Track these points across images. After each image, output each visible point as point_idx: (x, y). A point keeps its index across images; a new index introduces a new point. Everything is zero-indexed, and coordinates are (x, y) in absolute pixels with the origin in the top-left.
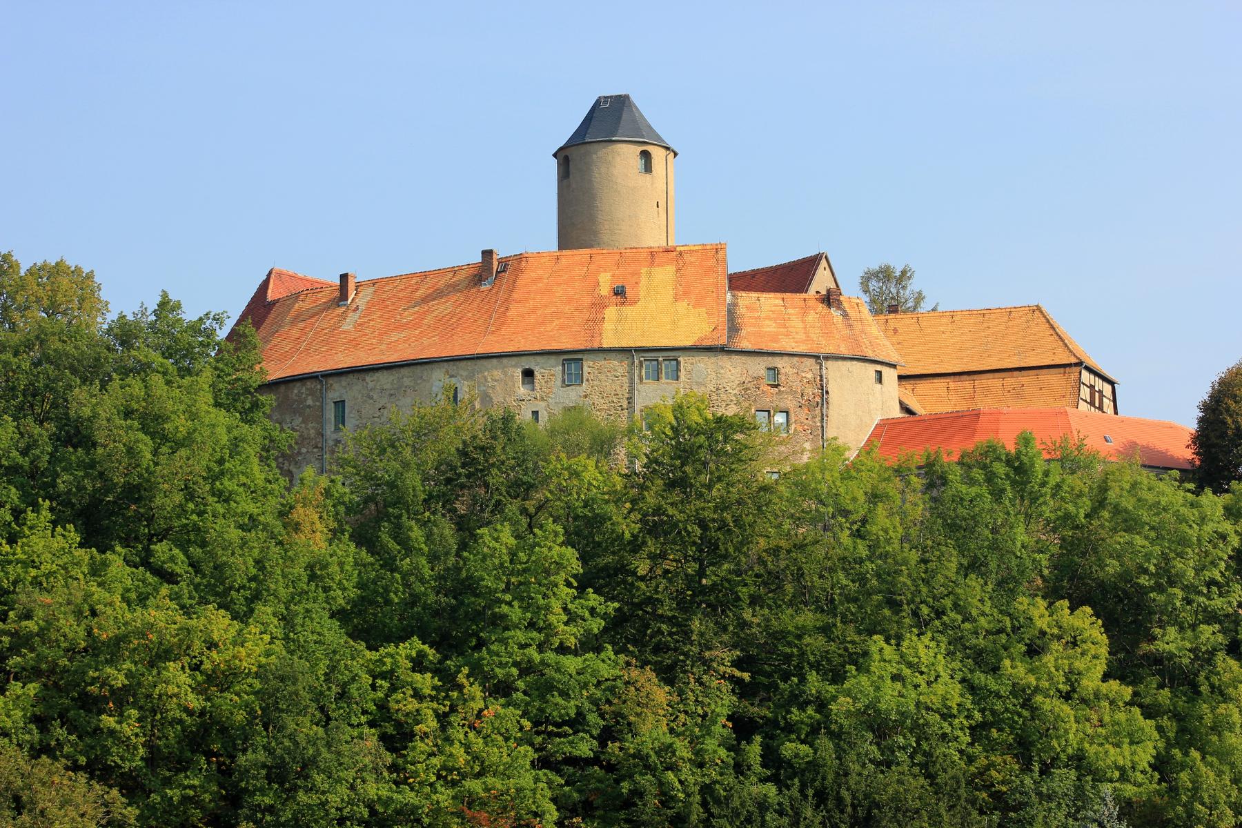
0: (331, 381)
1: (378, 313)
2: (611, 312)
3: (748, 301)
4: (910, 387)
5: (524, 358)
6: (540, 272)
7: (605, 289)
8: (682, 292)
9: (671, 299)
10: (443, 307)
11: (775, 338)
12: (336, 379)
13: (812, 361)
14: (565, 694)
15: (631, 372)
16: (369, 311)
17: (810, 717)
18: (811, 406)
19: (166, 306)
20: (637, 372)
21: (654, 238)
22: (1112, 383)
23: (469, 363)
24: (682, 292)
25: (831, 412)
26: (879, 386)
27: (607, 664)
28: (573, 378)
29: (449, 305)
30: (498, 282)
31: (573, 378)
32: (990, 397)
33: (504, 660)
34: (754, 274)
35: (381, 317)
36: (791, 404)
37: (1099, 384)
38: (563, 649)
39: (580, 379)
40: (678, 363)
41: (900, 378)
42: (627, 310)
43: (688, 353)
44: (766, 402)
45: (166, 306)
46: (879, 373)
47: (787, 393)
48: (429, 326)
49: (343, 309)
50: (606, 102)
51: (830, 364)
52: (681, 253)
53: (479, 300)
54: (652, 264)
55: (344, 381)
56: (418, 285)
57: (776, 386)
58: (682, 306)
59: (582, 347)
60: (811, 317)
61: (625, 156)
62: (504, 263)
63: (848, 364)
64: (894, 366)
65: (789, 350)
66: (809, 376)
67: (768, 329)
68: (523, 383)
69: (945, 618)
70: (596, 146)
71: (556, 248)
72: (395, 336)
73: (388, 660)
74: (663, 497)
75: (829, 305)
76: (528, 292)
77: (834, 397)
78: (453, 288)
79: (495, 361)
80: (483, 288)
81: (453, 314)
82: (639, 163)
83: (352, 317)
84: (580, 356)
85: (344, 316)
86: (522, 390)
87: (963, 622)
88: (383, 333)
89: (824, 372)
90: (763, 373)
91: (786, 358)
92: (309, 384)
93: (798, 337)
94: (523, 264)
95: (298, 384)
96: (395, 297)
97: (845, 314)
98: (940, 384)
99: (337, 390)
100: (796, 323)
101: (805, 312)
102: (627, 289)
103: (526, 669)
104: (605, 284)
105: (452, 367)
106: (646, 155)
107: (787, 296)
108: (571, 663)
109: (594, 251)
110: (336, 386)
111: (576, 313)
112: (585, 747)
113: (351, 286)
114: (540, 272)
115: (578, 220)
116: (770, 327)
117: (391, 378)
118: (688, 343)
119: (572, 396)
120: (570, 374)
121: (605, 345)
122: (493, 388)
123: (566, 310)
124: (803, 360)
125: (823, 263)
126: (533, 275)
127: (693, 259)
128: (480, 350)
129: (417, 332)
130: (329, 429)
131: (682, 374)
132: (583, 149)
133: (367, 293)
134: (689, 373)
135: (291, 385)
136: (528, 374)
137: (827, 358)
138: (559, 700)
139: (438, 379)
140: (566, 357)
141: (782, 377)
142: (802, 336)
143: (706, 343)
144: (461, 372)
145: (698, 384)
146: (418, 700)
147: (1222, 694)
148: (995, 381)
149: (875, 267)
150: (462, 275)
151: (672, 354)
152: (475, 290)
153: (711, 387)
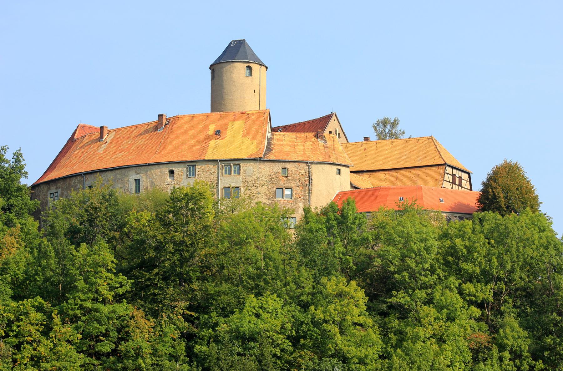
0: (87, 176)
1: (114, 144)
2: (212, 143)
3: (279, 137)
4: (367, 176)
5: (169, 165)
6: (184, 124)
7: (211, 131)
8: (247, 133)
9: (241, 136)
10: (141, 141)
11: (288, 154)
12: (89, 175)
13: (305, 164)
14: (99, 322)
17: (210, 333)
18: (303, 186)
20: (220, 171)
21: (242, 110)
22: (469, 174)
23: (145, 167)
24: (247, 133)
25: (313, 189)
26: (339, 176)
27: (123, 308)
28: (192, 174)
29: (143, 140)
30: (165, 129)
32: (405, 180)
33: (74, 307)
34: (305, 123)
35: (115, 147)
36: (293, 185)
37: (458, 174)
38: (104, 301)
39: (194, 174)
40: (240, 166)
41: (351, 172)
42: (220, 141)
43: (244, 162)
44: (281, 184)
46: (339, 170)
47: (292, 180)
48: (133, 150)
49: (101, 143)
50: (234, 43)
52: (248, 114)
53: (156, 138)
54: (234, 120)
56: (133, 131)
57: (287, 177)
59: (196, 160)
60: (308, 144)
61: (239, 68)
62: (169, 120)
63: (323, 166)
64: (348, 167)
65: (293, 159)
67: (286, 150)
68: (170, 177)
69: (288, 287)
70: (225, 64)
71: (210, 112)
72: (119, 155)
73: (22, 307)
74: (329, 229)
75: (318, 138)
76: (177, 134)
78: (146, 132)
79: (156, 166)
80: (158, 132)
81: (144, 144)
82: (245, 71)
83: (104, 146)
84: (195, 164)
86: (169, 180)
87: (296, 289)
88: (114, 154)
89: (310, 170)
90: (280, 170)
91: (292, 164)
92: (79, 178)
93: (299, 153)
94: (176, 120)
95: (74, 178)
96: (123, 137)
97: (325, 142)
98: (382, 174)
100: (300, 146)
101: (305, 141)
102: (221, 132)
105: (138, 169)
106: (249, 68)
107: (297, 134)
109: (222, 113)
110: (89, 179)
111: (197, 143)
113: (105, 132)
114: (184, 124)
115: (218, 101)
116: (287, 149)
117: (112, 175)
120: (190, 172)
121: (206, 159)
122: (156, 179)
123: (193, 142)
124: (300, 164)
125: (334, 116)
126: (180, 126)
127: (253, 117)
128: (151, 161)
129: (127, 153)
131: (242, 172)
132: (219, 66)
133: (112, 135)
135: (72, 178)
136: (172, 172)
137: (312, 163)
138: (98, 325)
139: (132, 176)
140: (188, 164)
141: (289, 173)
143: (253, 157)
144: (142, 172)
145: (249, 176)
147: (420, 322)
148: (407, 172)
149: (381, 118)
150: (152, 125)
151: (237, 162)
152: (155, 133)
153: (255, 177)
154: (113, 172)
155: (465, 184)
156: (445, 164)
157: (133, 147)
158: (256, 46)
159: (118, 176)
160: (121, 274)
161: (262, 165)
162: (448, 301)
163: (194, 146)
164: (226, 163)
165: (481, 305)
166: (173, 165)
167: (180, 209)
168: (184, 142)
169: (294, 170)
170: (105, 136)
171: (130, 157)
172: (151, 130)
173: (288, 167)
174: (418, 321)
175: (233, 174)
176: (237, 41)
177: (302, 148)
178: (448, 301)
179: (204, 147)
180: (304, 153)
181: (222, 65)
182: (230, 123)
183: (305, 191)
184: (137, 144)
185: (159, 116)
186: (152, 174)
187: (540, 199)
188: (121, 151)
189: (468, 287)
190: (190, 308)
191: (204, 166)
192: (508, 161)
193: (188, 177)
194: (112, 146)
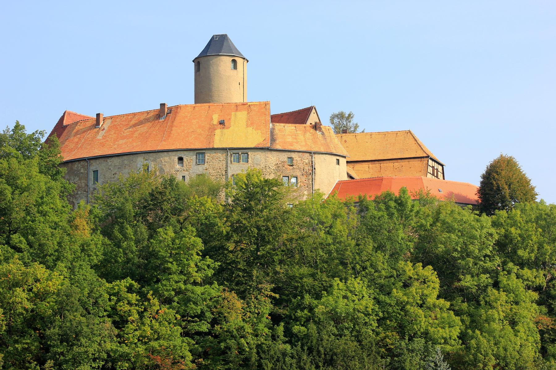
0: (92, 162)
2: (218, 132)
3: (279, 127)
4: (352, 166)
5: (179, 152)
7: (215, 121)
8: (250, 123)
9: (245, 126)
11: (291, 144)
12: (94, 161)
13: (308, 154)
14: (195, 303)
15: (227, 159)
16: (109, 130)
18: (307, 174)
19: (18, 127)
20: (229, 159)
22: (442, 165)
23: (154, 154)
24: (250, 123)
25: (316, 178)
27: (215, 290)
28: (201, 161)
29: (145, 128)
30: (167, 118)
31: (201, 161)
32: (388, 171)
33: (168, 288)
35: (115, 133)
36: (298, 174)
37: (436, 166)
38: (195, 283)
39: (204, 162)
40: (248, 155)
41: (347, 162)
42: (225, 131)
44: (287, 173)
45: (18, 127)
46: (338, 160)
48: (136, 137)
49: (98, 129)
50: (216, 38)
51: (316, 156)
52: (249, 106)
53: (159, 126)
54: (237, 110)
55: (98, 161)
58: (250, 129)
59: (205, 148)
60: (308, 135)
61: (225, 62)
62: (170, 109)
63: (324, 156)
64: (345, 157)
65: (298, 149)
66: (307, 161)
67: (289, 140)
69: (367, 271)
72: (121, 142)
73: (116, 288)
75: (316, 129)
77: (318, 170)
78: (147, 120)
79: (165, 153)
80: (161, 120)
81: (147, 132)
83: (102, 133)
84: (204, 151)
85: (98, 132)
86: (178, 167)
89: (313, 159)
90: (286, 159)
91: (296, 153)
92: (82, 163)
95: (77, 163)
97: (323, 134)
98: (365, 165)
99: (94, 166)
100: (301, 137)
102: (226, 122)
103: (178, 292)
104: (216, 119)
105: (146, 156)
106: (234, 61)
108: (199, 290)
109: (210, 104)
110: (94, 164)
111: (202, 132)
112: (205, 327)
113: (101, 119)
114: (187, 114)
115: (204, 90)
116: (289, 139)
117: (119, 160)
118: (253, 146)
119: (200, 169)
122: (165, 165)
124: (304, 154)
126: (183, 115)
127: (255, 108)
128: (159, 148)
129: (131, 140)
130: (91, 183)
131: (250, 160)
132: (206, 59)
133: (108, 122)
134: (253, 159)
135: (74, 163)
136: (181, 159)
137: (315, 153)
138: (193, 306)
141: (295, 162)
142: (303, 143)
143: (261, 146)
144: (151, 158)
145: (257, 164)
146: (130, 305)
148: (390, 164)
149: (337, 112)
150: (152, 114)
152: (157, 121)
153: (263, 165)
154: (120, 158)
155: (440, 175)
156: (428, 157)
157: (136, 134)
158: (235, 39)
159: (126, 162)
160: (208, 257)
161: (269, 154)
162: (514, 286)
163: (200, 134)
164: (234, 151)
165: (538, 289)
166: (182, 152)
167: (255, 195)
168: (190, 131)
169: (299, 159)
170: (101, 123)
171: (135, 144)
172: (152, 119)
173: (293, 157)
174: (489, 305)
175: (241, 163)
176: (219, 35)
177: (303, 139)
178: (514, 286)
179: (210, 135)
180: (306, 144)
181: (208, 57)
182: (233, 113)
183: (309, 180)
184: (139, 132)
185: (161, 105)
186: (161, 161)
187: (536, 190)
188: (123, 138)
189: (527, 272)
190: (273, 290)
191: (213, 154)
192: (504, 155)
193: (197, 164)
194: (112, 133)
